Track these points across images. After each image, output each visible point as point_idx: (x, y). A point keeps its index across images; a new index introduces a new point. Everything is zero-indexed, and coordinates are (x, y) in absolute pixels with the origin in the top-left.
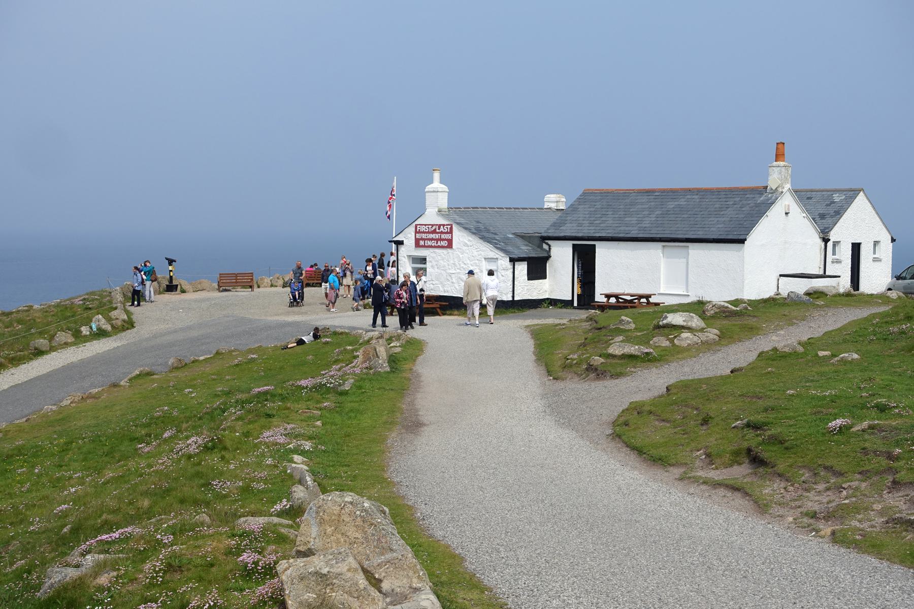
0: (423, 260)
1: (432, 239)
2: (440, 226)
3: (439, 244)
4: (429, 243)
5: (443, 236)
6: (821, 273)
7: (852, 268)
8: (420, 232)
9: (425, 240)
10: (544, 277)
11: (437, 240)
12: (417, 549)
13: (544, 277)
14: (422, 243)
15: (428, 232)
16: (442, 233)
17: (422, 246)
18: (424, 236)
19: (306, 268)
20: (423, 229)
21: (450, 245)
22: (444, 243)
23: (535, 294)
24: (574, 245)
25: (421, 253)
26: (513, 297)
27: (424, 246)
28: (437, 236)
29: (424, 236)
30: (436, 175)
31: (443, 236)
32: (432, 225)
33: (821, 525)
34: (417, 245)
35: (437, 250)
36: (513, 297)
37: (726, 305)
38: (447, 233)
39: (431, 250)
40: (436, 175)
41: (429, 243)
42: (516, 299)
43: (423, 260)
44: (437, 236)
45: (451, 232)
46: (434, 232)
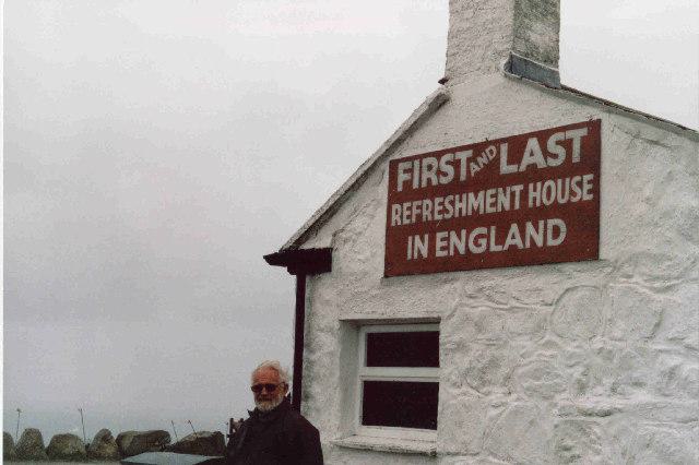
0: (420, 344)
1: (476, 219)
2: (517, 145)
3: (514, 238)
4: (458, 243)
5: (538, 194)
7: (295, 363)
11: (501, 221)
13: (434, 427)
15: (442, 191)
16: (535, 175)
18: (431, 209)
19: (236, 420)
25: (411, 302)
29: (431, 209)
31: (538, 194)
32: (478, 149)
34: (398, 265)
38: (566, 171)
39: (463, 283)
41: (458, 243)
43: (420, 344)
45: (590, 160)
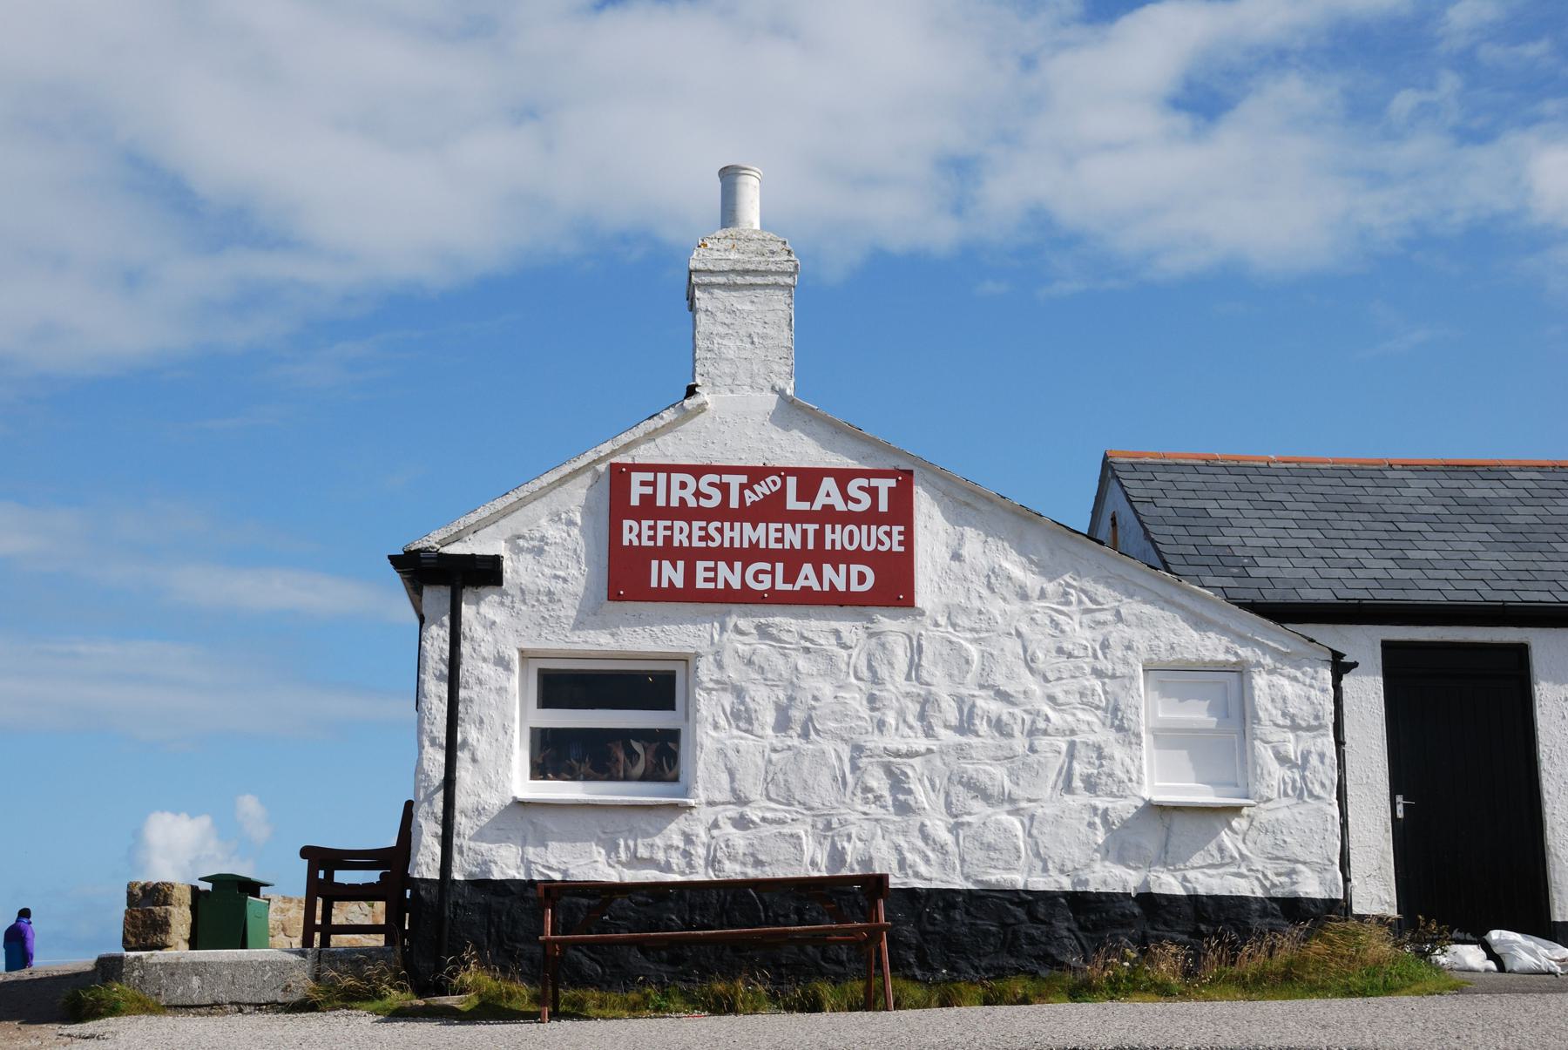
1: (751, 554)
4: (730, 576)
5: (836, 537)
8: (648, 509)
9: (690, 556)
10: (533, 777)
11: (792, 560)
12: (1089, 909)
13: (533, 777)
15: (723, 513)
16: (828, 515)
18: (683, 534)
23: (442, 633)
24: (1387, 646)
25: (640, 638)
27: (688, 594)
29: (683, 534)
31: (836, 537)
32: (756, 474)
34: (626, 578)
35: (786, 622)
38: (871, 517)
41: (730, 576)
43: (655, 686)
45: (901, 511)
46: (772, 509)
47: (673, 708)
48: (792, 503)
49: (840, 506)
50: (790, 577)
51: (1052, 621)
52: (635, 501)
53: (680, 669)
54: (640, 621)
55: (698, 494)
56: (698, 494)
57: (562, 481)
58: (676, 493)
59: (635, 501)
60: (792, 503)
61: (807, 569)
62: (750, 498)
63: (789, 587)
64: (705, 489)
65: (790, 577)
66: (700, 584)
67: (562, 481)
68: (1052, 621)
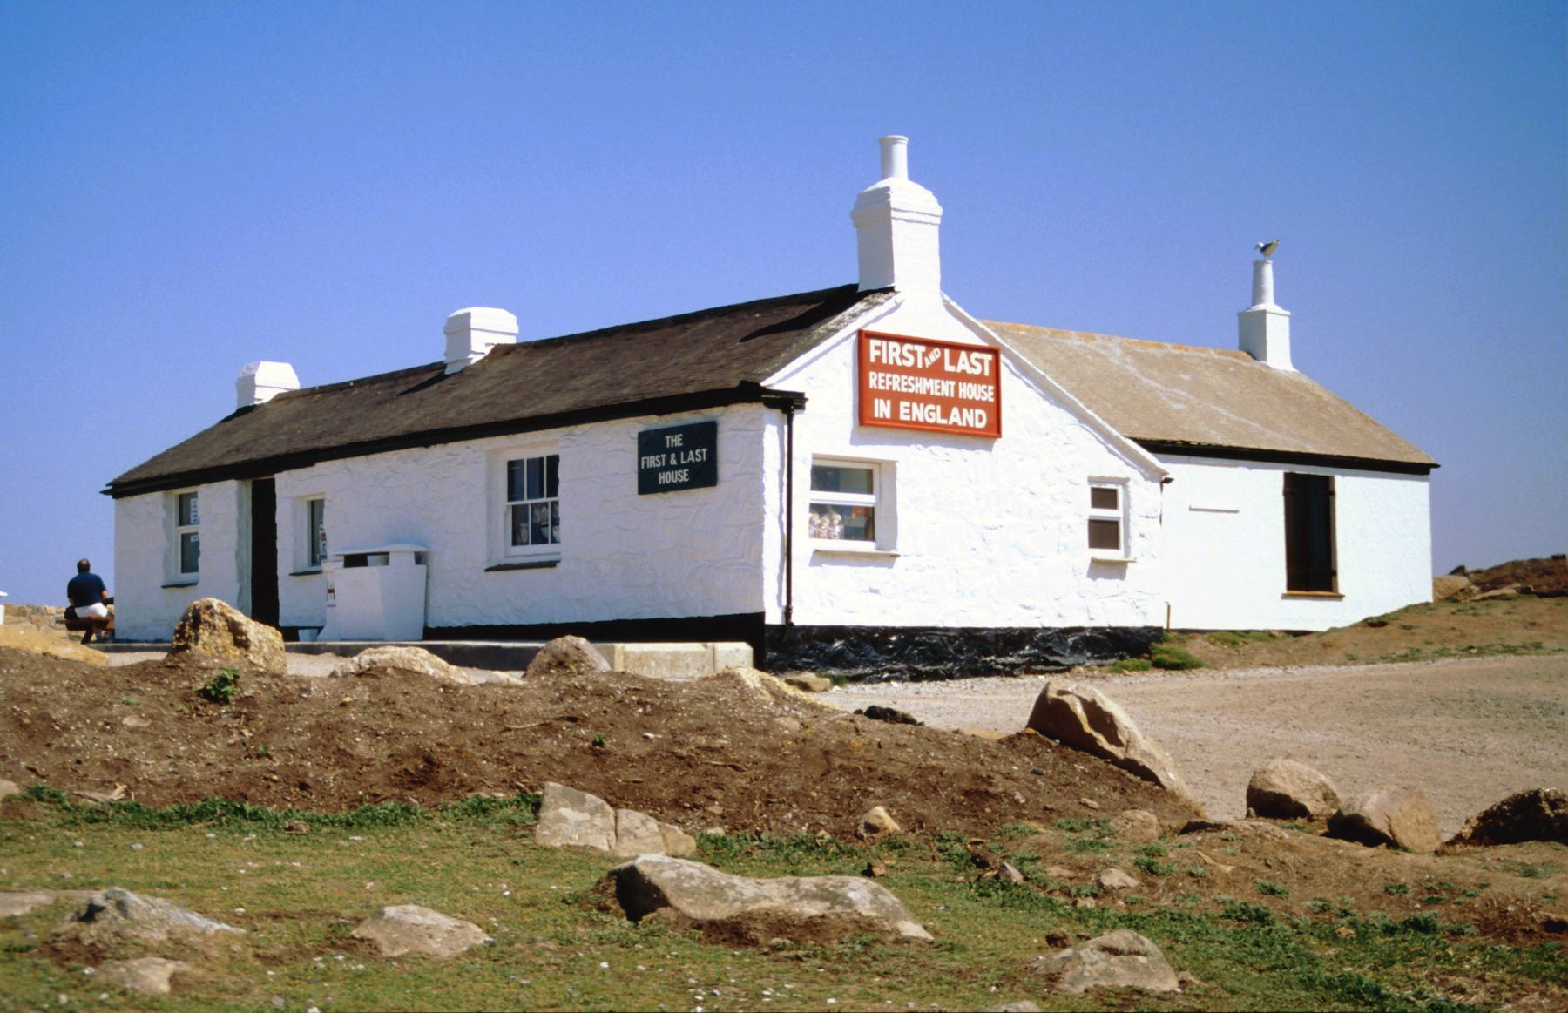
1: (925, 399)
3: (955, 417)
4: (920, 413)
6: (290, 487)
11: (947, 404)
14: (882, 409)
15: (913, 371)
16: (963, 377)
17: (882, 424)
20: (892, 353)
21: (994, 429)
22: (975, 419)
26: (788, 612)
28: (945, 388)
30: (900, 151)
32: (930, 344)
33: (674, 946)
36: (788, 612)
37: (1079, 710)
38: (978, 380)
40: (900, 151)
42: (797, 620)
44: (945, 388)
45: (996, 379)
46: (936, 371)
47: (183, 571)
48: (948, 368)
49: (970, 371)
50: (946, 414)
51: (1105, 949)
52: (873, 360)
53: (1120, 489)
54: (897, 442)
55: (902, 357)
56: (902, 357)
57: (839, 343)
58: (892, 354)
59: (873, 360)
60: (948, 368)
61: (955, 410)
62: (928, 363)
63: (944, 422)
64: (906, 354)
65: (946, 414)
66: (903, 417)
67: (839, 343)
68: (1105, 949)
